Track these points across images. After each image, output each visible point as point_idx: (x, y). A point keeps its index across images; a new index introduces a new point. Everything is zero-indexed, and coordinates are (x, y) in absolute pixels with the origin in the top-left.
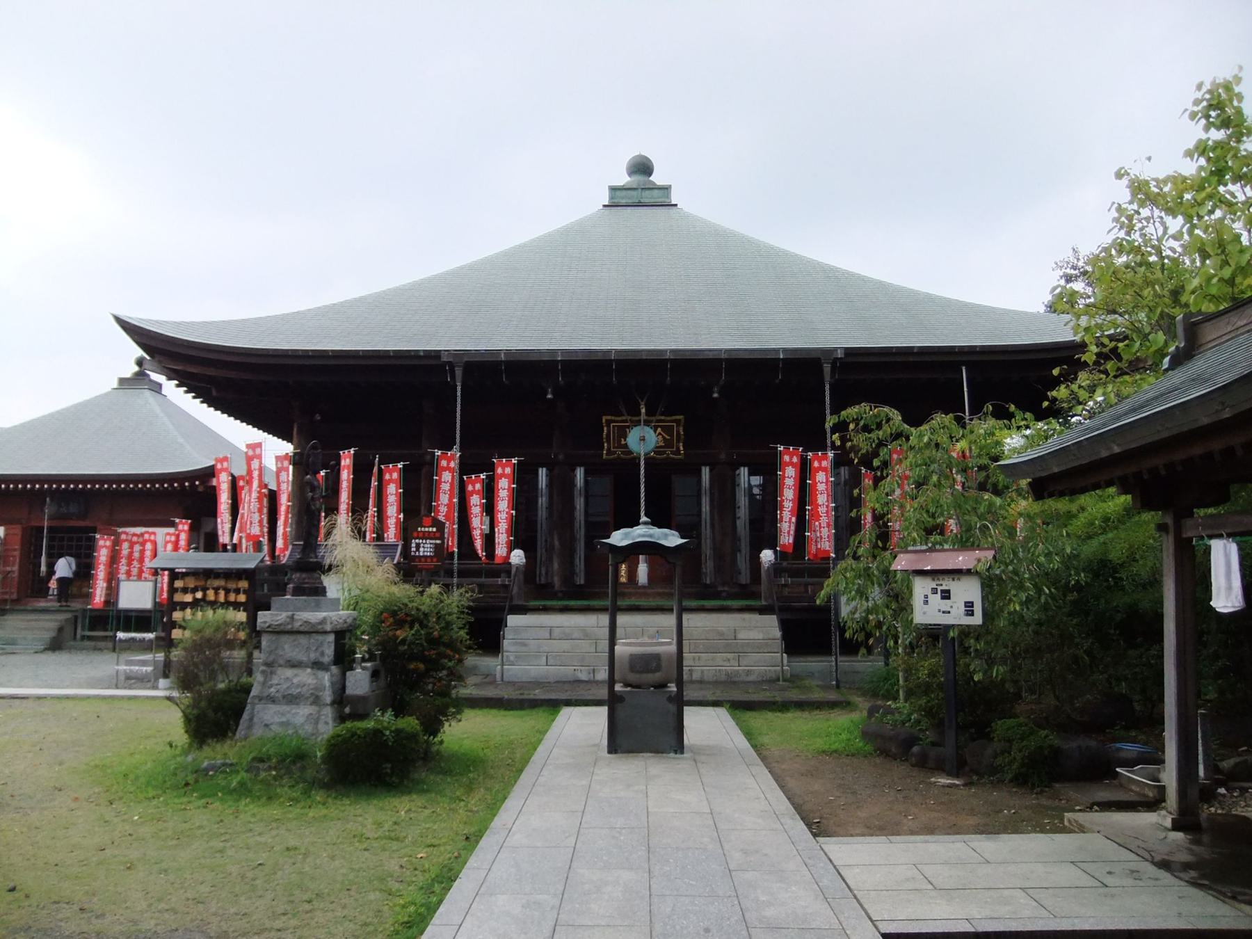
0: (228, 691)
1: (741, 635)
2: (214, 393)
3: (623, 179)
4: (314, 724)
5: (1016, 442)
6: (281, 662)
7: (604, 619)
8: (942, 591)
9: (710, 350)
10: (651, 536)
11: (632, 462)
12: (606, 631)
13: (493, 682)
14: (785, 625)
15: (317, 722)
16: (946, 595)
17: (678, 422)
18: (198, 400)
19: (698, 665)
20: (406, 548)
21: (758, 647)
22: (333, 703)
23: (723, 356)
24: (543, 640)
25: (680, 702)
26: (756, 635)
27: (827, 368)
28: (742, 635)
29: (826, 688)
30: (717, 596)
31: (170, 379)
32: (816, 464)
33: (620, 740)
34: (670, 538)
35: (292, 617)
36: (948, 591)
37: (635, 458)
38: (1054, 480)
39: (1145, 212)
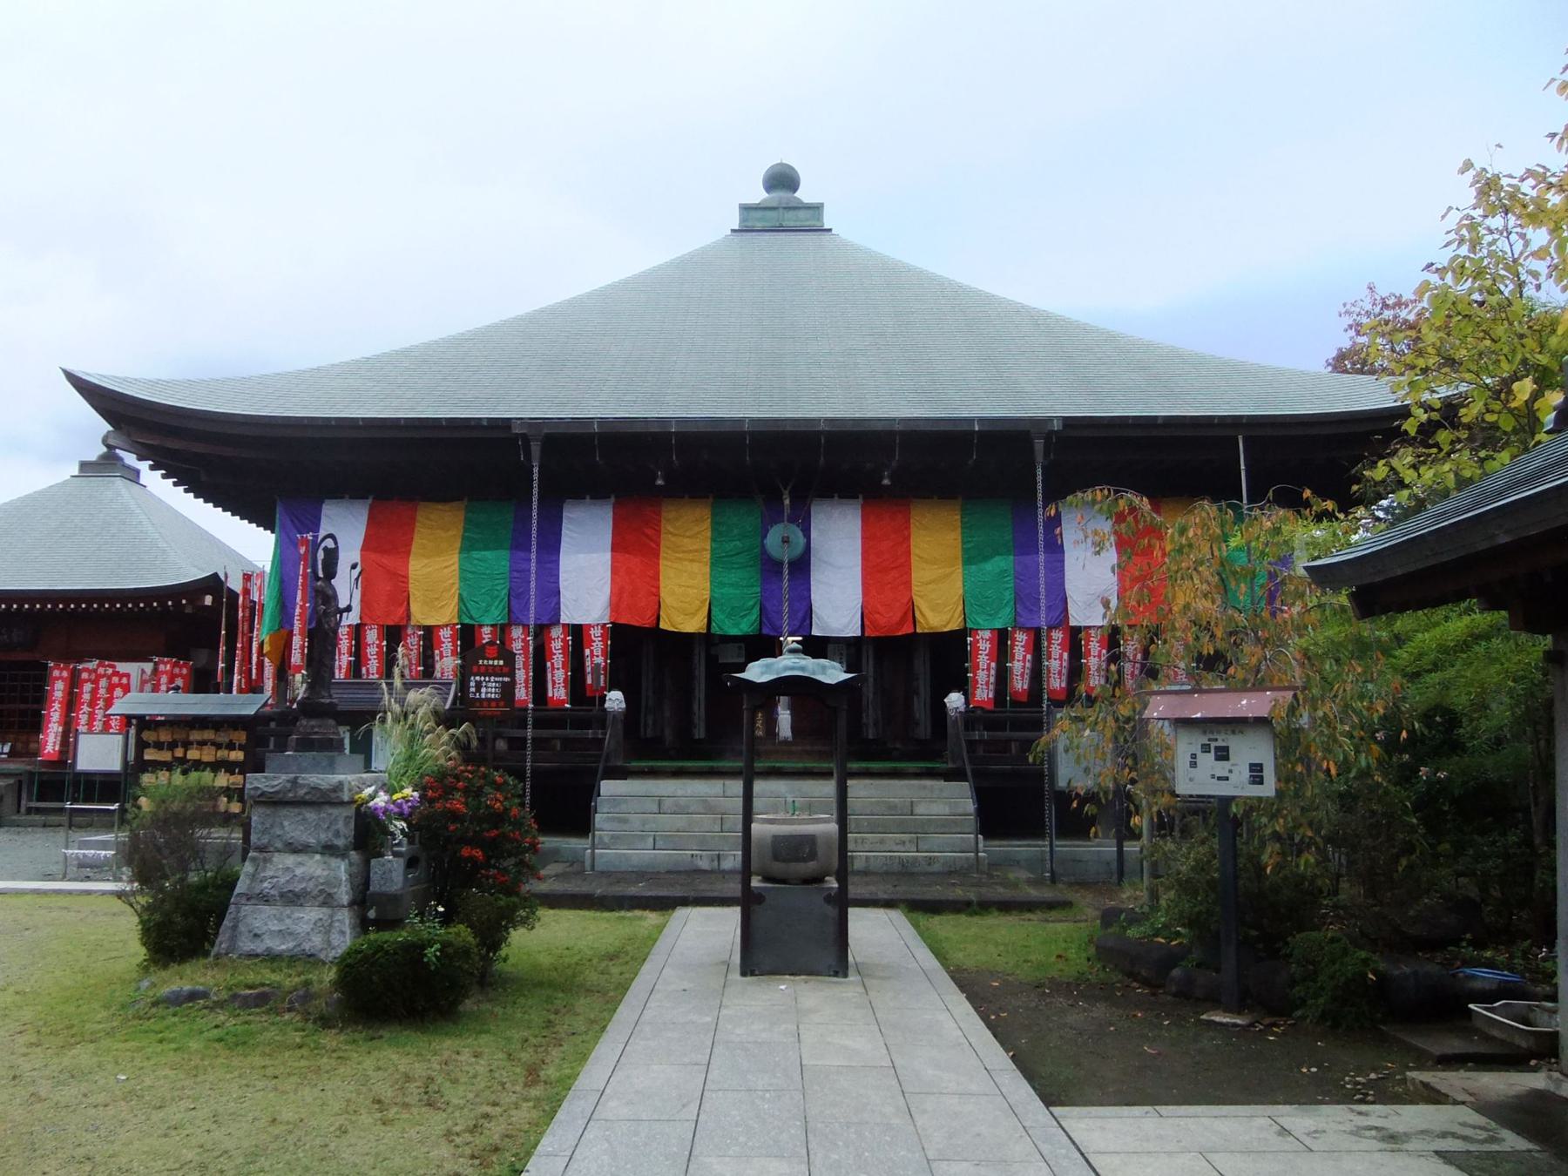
0: (202, 888)
1: (920, 809)
2: (204, 478)
3: (758, 195)
4: (326, 932)
5: (1313, 539)
6: (279, 845)
7: (736, 786)
8: (1217, 748)
9: (879, 420)
10: (803, 669)
12: (739, 802)
13: (580, 873)
14: (981, 796)
15: (328, 930)
16: (1223, 754)
18: (181, 488)
19: (866, 850)
20: (463, 686)
21: (945, 826)
22: (351, 904)
23: (897, 427)
24: (649, 816)
25: (842, 902)
26: (939, 809)
27: (1039, 444)
28: (920, 809)
29: (1037, 883)
30: (885, 755)
31: (141, 458)
33: (760, 955)
34: (830, 671)
35: (294, 782)
38: (1380, 589)
39: (1497, 222)
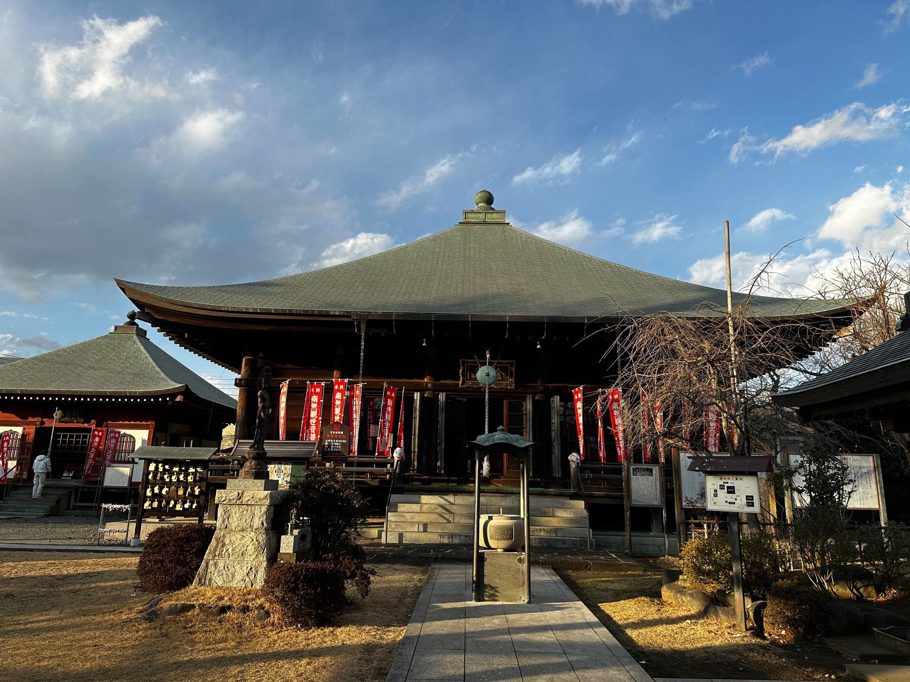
10: (167, 454)
11: (480, 391)
16: (731, 490)
17: (511, 364)
32: (336, 387)
36: (733, 488)
37: (481, 388)
